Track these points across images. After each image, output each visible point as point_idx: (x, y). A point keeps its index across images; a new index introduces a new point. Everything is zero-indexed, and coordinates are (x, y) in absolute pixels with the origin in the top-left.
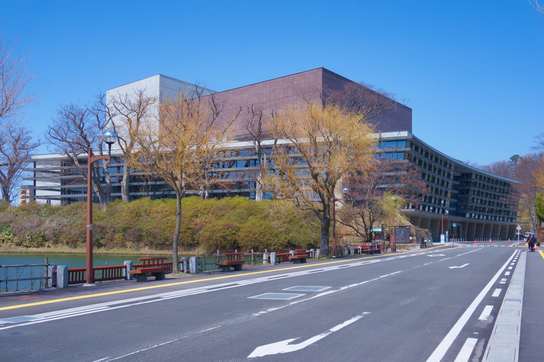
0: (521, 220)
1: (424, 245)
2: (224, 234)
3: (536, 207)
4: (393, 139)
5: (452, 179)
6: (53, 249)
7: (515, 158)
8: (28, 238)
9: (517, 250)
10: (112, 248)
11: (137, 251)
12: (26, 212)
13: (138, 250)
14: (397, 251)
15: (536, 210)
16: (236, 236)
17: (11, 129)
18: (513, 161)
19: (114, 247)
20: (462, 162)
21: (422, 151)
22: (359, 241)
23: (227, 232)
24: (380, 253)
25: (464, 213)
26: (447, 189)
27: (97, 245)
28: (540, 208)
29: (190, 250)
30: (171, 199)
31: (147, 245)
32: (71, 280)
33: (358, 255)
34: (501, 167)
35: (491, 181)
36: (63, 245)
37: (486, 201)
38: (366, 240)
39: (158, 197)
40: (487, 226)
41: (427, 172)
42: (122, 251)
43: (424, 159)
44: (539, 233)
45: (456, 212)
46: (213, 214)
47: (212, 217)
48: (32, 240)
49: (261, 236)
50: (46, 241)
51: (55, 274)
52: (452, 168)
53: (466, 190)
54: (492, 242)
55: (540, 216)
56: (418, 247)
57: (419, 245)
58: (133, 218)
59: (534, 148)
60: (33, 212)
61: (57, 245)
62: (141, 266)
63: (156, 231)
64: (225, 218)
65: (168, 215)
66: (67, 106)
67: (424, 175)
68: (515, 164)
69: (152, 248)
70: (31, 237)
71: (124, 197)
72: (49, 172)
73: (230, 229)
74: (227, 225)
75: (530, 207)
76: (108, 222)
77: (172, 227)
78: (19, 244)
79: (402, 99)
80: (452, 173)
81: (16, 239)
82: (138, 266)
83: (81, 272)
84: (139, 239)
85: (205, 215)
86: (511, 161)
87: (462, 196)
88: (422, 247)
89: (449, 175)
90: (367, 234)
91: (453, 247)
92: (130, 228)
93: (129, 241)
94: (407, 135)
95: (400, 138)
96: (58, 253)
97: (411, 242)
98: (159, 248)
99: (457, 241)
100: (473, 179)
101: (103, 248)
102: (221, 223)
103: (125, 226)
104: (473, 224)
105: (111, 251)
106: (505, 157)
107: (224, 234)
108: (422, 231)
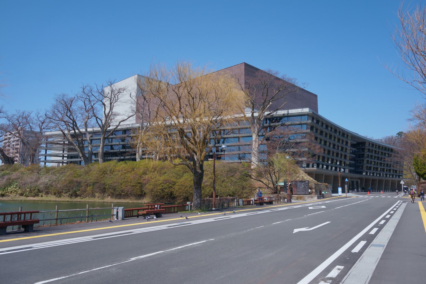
0: (407, 177)
1: (321, 196)
2: (162, 188)
3: (415, 166)
4: (297, 114)
5: (350, 146)
6: (45, 198)
7: (400, 134)
8: (28, 190)
9: (399, 201)
10: (85, 198)
11: (102, 200)
12: (30, 171)
13: (103, 199)
14: (292, 201)
15: (415, 168)
16: (172, 189)
17: (39, 115)
18: (399, 136)
19: (86, 197)
20: (358, 134)
21: (323, 124)
22: (269, 193)
23: (165, 186)
24: (272, 204)
25: (361, 172)
26: (346, 153)
27: (75, 195)
28: (418, 166)
29: (139, 199)
30: (131, 161)
31: (110, 195)
32: (126, 215)
33: (251, 206)
34: (390, 140)
35: (381, 148)
36: (52, 195)
37: (371, 161)
38: (274, 192)
39: (122, 160)
40: (380, 181)
41: (319, 136)
42: (92, 200)
43: (324, 130)
44: (419, 186)
45: (355, 171)
46: (158, 172)
47: (157, 174)
48: (31, 191)
49: (191, 189)
50: (40, 192)
51: (117, 212)
52: (349, 138)
53: (362, 154)
54: (383, 193)
55: (418, 173)
56: (316, 198)
57: (317, 196)
58: (101, 175)
59: (410, 119)
60: (35, 171)
61: (48, 195)
62: (147, 209)
63: (115, 185)
64: (166, 174)
65: (125, 173)
66: (60, 95)
67: (316, 138)
68: (401, 138)
69: (113, 198)
70: (30, 189)
71: (100, 160)
72: (58, 144)
73: (168, 183)
74: (165, 180)
75: (410, 166)
76: (83, 178)
77: (127, 182)
78: (22, 195)
79: (302, 83)
80: (349, 142)
81: (20, 191)
82: (145, 209)
83: (132, 211)
84: (103, 191)
85: (152, 173)
86: (398, 136)
87: (359, 159)
88: (319, 197)
89: (347, 143)
90: (274, 188)
91: (346, 197)
92: (98, 183)
93: (97, 192)
94: (308, 111)
95: (303, 113)
96: (47, 201)
97: (310, 193)
98: (118, 198)
99: (352, 192)
100: (367, 146)
101: (79, 197)
102: (162, 178)
103: (94, 181)
104: (369, 179)
105: (83, 200)
106: (394, 133)
107: (162, 188)
108: (321, 184)
